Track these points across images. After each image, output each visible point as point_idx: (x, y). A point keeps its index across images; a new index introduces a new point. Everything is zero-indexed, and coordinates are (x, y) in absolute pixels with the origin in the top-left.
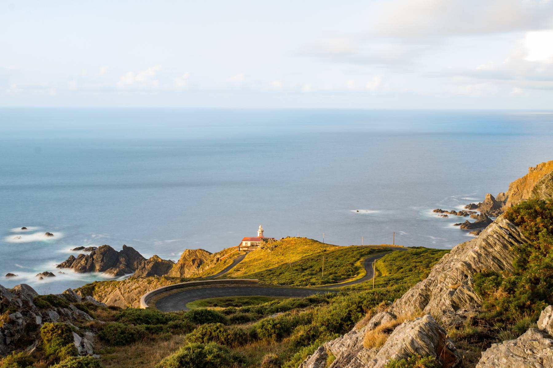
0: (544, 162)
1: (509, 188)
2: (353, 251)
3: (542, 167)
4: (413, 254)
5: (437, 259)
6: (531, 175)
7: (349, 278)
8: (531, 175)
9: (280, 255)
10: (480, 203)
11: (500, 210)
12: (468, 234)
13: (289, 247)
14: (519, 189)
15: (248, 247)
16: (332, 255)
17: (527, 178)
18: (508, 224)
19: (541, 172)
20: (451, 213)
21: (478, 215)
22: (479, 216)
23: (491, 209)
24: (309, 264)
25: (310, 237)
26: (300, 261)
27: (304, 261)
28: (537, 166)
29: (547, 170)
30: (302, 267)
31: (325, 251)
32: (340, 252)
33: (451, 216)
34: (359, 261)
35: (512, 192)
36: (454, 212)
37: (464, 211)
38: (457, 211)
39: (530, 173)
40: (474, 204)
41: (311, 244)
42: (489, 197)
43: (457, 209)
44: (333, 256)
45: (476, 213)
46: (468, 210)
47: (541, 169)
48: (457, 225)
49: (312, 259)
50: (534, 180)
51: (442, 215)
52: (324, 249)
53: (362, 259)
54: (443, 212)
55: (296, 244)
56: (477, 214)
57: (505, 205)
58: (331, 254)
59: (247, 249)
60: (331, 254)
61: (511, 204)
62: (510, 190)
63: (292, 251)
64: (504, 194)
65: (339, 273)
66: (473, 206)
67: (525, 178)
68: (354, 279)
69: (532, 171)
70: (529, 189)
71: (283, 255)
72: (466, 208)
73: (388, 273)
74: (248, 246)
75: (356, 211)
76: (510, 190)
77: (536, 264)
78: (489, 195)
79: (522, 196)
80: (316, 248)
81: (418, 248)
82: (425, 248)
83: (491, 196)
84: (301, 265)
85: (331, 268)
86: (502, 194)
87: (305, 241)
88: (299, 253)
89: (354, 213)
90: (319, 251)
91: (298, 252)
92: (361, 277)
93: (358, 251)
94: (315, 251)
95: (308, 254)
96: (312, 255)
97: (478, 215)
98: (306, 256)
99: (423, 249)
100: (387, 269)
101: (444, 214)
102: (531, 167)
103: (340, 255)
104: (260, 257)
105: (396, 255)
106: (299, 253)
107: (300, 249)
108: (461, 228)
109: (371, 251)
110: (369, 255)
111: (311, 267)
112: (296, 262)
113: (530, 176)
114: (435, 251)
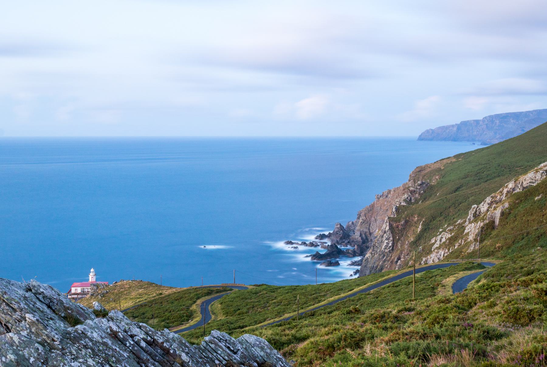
0: (389, 189)
1: (357, 216)
2: (190, 293)
3: (388, 194)
4: (253, 294)
5: (276, 297)
6: (378, 203)
7: (183, 324)
8: (378, 203)
9: (111, 302)
10: (329, 233)
11: (350, 239)
12: (319, 266)
13: (122, 292)
14: (367, 217)
15: (78, 294)
16: (168, 298)
17: (374, 205)
18: (382, 251)
19: (387, 199)
20: (301, 244)
21: (328, 245)
22: (329, 247)
23: (340, 239)
24: (142, 310)
25: (146, 280)
26: (132, 307)
27: (136, 307)
28: (383, 193)
29: (392, 197)
30: (133, 314)
31: (161, 294)
32: (177, 295)
33: (302, 248)
34: (194, 305)
35: (361, 221)
36: (304, 243)
37: (314, 242)
38: (307, 243)
39: (377, 201)
40: (324, 235)
41: (147, 287)
42: (339, 226)
43: (307, 241)
44: (168, 300)
45: (326, 243)
46: (317, 240)
47: (387, 196)
48: (307, 256)
49: (145, 305)
50: (381, 208)
51: (292, 247)
52: (160, 292)
53: (199, 302)
54: (292, 243)
55: (130, 287)
56: (327, 245)
57: (354, 234)
58: (167, 298)
59: (76, 296)
60: (167, 298)
61: (360, 233)
62: (358, 218)
63: (125, 297)
64: (353, 222)
65: (173, 319)
66: (322, 237)
67: (372, 206)
68: (188, 325)
69: (379, 198)
70: (377, 216)
71: (114, 301)
72: (316, 238)
73: (225, 316)
74: (78, 292)
75: (203, 247)
76: (358, 218)
77: (228, 331)
78: (338, 225)
79: (370, 224)
80: (152, 292)
81: (260, 286)
82: (267, 285)
83: (340, 224)
84: (133, 312)
85: (164, 313)
86: (350, 223)
87: (141, 285)
88: (132, 299)
89: (201, 248)
90: (155, 295)
91: (131, 297)
92: (195, 323)
93: (195, 293)
94: (149, 295)
95: (141, 299)
96: (146, 299)
97: (328, 245)
98: (139, 302)
99: (264, 287)
100: (223, 312)
101: (294, 245)
102: (377, 194)
103: (176, 299)
104: (90, 305)
105: (235, 295)
106: (132, 299)
107: (134, 294)
108: (312, 258)
109: (208, 292)
110: (206, 297)
111: (144, 314)
112: (129, 309)
113: (376, 204)
114: (276, 289)
